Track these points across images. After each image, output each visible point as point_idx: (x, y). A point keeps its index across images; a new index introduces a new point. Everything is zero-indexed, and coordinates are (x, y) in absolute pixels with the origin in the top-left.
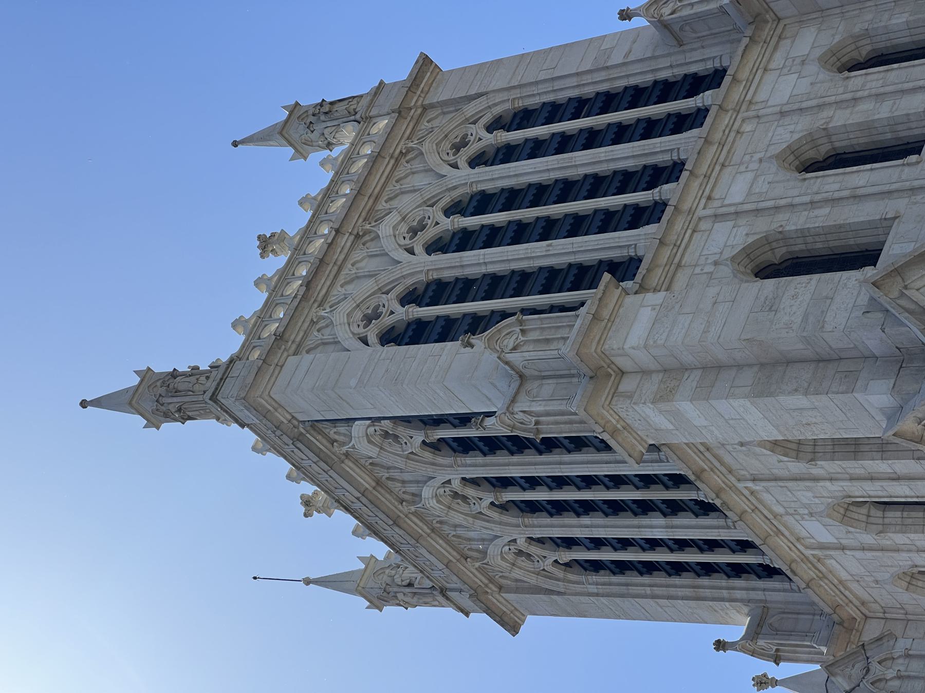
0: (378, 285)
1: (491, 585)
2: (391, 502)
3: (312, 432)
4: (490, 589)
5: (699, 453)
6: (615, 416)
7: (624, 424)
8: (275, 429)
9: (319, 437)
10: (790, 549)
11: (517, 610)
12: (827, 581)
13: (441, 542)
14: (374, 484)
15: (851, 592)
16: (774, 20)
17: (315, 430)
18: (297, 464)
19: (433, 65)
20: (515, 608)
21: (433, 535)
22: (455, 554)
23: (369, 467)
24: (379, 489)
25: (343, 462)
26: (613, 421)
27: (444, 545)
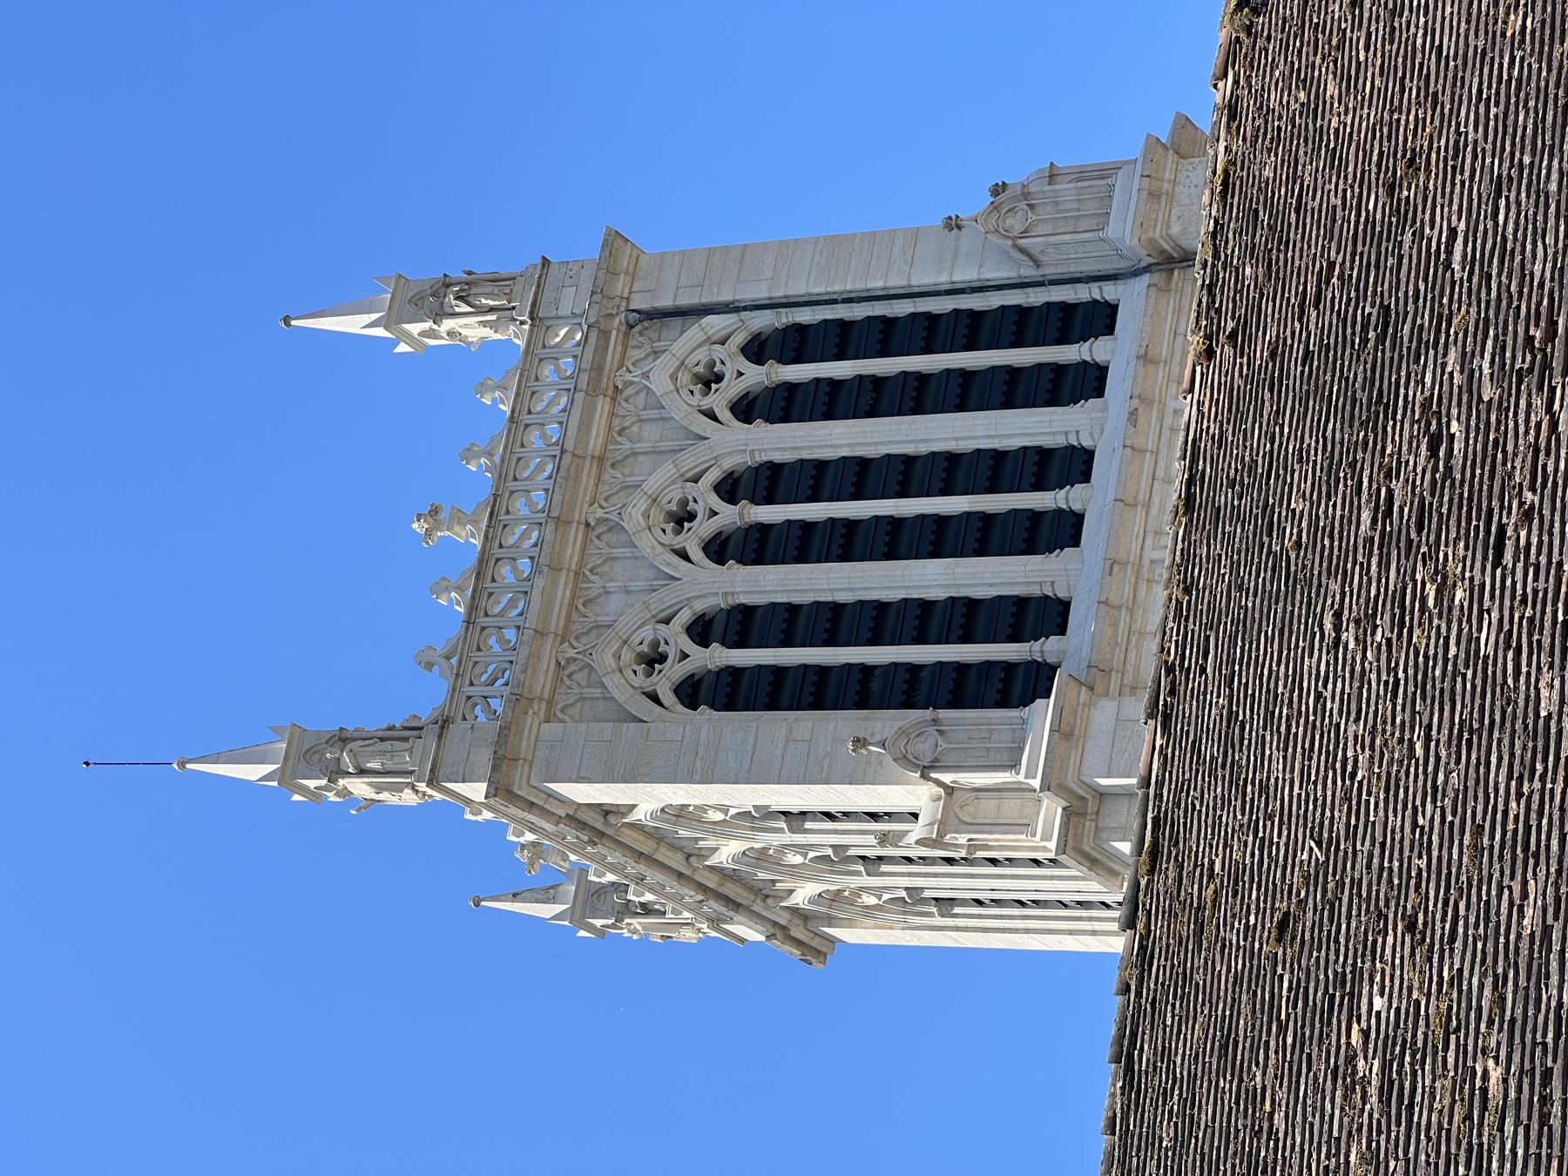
0: (829, 584)
1: (544, 705)
2: (586, 490)
3: (621, 336)
4: (539, 708)
5: (1173, 333)
6: (1173, 173)
7: (1170, 190)
8: (599, 291)
9: (619, 348)
10: (1137, 537)
11: (531, 767)
12: (1128, 619)
13: (568, 592)
14: (597, 454)
15: (1139, 657)
16: (1094, 797)
17: (624, 337)
18: (516, 415)
19: (1200, 132)
20: (532, 761)
21: (572, 574)
22: (562, 623)
23: (615, 434)
24: (595, 464)
25: (605, 396)
26: (1167, 175)
27: (566, 601)
